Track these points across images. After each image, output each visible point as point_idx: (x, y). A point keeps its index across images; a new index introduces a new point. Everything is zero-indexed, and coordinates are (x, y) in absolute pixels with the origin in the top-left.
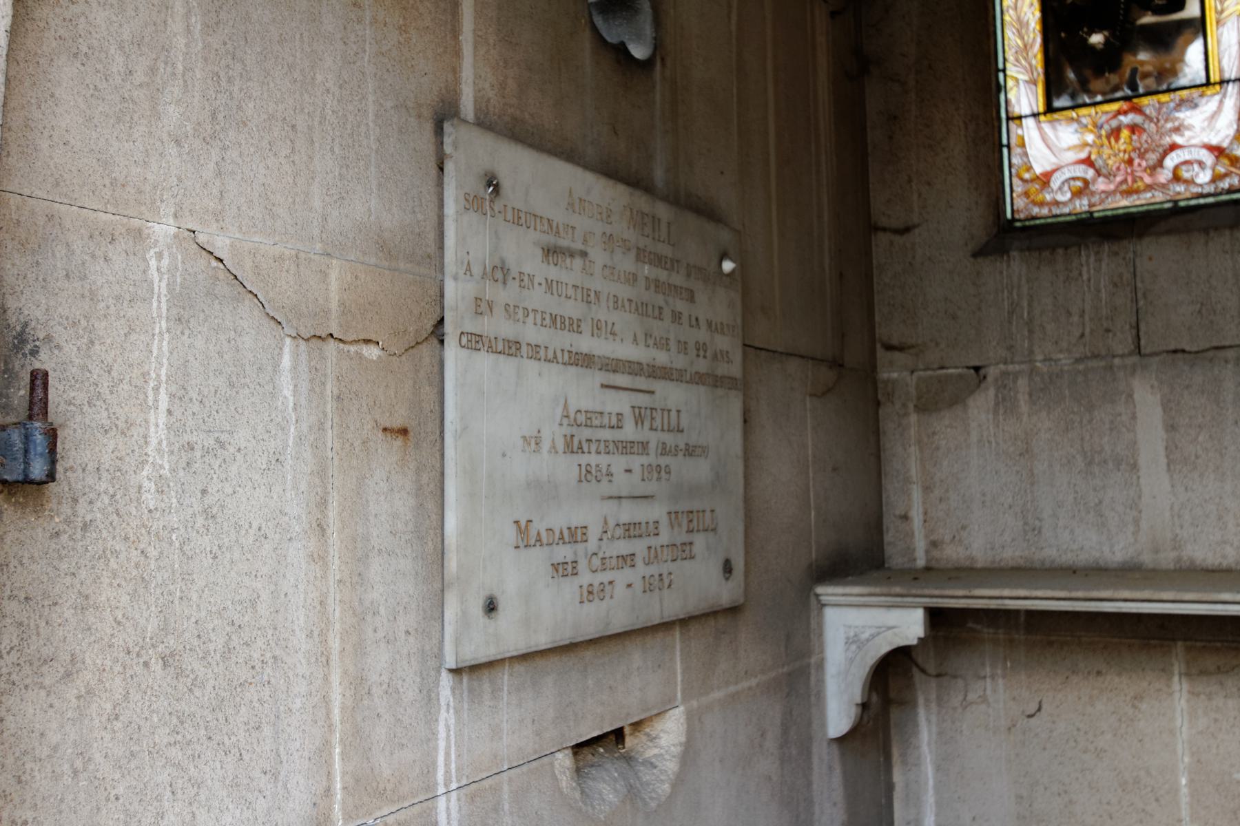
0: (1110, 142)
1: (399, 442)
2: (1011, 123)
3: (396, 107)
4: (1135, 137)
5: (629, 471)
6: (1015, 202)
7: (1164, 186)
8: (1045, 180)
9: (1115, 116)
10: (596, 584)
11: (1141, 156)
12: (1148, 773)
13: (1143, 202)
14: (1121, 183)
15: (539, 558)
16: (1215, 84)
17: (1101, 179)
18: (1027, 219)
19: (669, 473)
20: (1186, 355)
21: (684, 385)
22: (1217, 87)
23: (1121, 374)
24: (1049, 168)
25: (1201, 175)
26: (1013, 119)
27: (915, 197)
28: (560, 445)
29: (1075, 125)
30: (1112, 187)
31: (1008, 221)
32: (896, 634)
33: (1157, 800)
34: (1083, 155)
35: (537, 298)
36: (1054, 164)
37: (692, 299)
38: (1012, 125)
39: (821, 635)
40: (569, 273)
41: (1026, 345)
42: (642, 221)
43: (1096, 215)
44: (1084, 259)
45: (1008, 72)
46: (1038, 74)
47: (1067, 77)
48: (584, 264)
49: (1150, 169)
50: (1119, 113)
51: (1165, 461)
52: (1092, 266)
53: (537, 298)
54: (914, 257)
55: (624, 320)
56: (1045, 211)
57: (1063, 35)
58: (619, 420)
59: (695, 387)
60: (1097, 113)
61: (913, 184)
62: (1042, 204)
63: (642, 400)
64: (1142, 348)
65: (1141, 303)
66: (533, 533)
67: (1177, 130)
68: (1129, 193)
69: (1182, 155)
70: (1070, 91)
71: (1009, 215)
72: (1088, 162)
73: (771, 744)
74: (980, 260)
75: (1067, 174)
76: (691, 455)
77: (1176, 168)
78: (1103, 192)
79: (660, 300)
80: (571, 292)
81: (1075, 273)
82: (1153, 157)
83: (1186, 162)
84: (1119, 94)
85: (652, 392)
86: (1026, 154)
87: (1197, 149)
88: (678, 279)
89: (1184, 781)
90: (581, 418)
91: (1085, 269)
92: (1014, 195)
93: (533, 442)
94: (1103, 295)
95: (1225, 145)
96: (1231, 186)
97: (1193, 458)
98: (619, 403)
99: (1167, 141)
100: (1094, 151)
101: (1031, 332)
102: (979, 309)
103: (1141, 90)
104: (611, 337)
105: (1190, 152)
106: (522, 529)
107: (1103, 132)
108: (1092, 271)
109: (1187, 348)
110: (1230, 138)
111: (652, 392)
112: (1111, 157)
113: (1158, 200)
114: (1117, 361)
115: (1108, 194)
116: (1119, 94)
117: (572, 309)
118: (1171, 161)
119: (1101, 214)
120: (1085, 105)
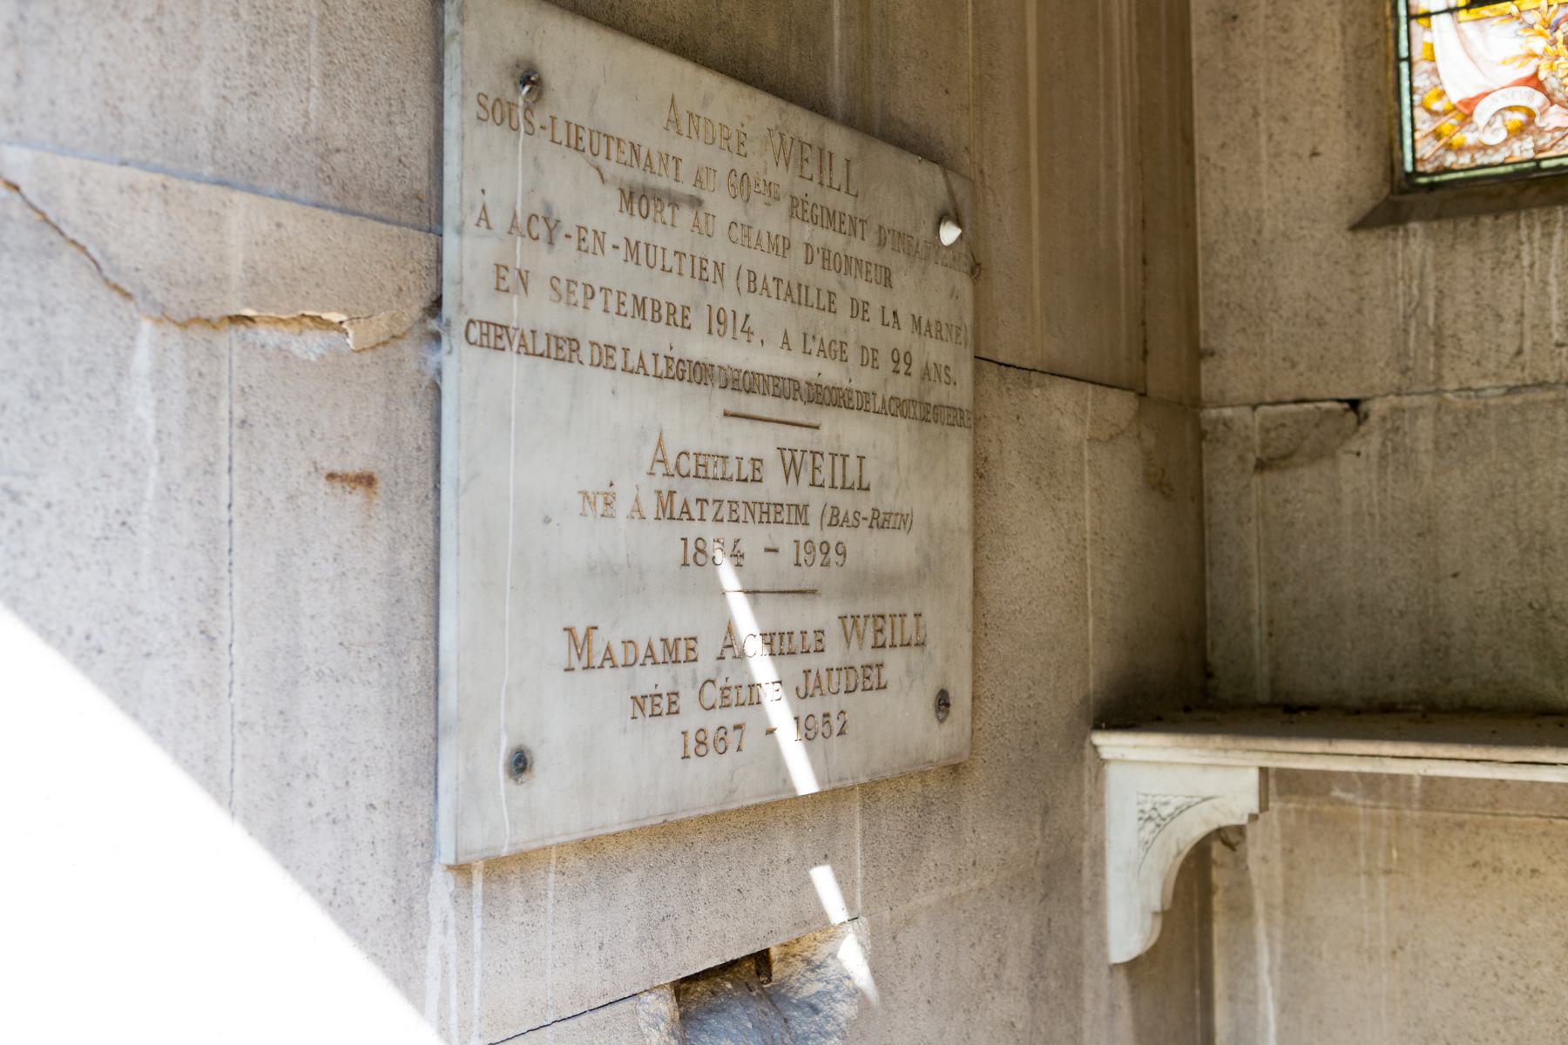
6: (1418, 145)
8: (1465, 110)
15: (610, 688)
18: (1437, 172)
21: (873, 416)
27: (1263, 139)
28: (650, 506)
29: (1515, 25)
32: (1215, 808)
34: (1527, 72)
37: (888, 282)
41: (1431, 367)
42: (798, 154)
43: (1545, 164)
44: (1524, 232)
52: (1536, 245)
53: (609, 269)
54: (1260, 232)
55: (766, 311)
56: (1465, 160)
61: (1260, 120)
62: (1460, 150)
63: (795, 438)
72: (1534, 82)
74: (1362, 235)
78: (1558, 129)
81: (1509, 256)
86: (1435, 71)
91: (1526, 248)
92: (1418, 135)
100: (1544, 64)
101: (1439, 345)
102: (1359, 311)
108: (1537, 252)
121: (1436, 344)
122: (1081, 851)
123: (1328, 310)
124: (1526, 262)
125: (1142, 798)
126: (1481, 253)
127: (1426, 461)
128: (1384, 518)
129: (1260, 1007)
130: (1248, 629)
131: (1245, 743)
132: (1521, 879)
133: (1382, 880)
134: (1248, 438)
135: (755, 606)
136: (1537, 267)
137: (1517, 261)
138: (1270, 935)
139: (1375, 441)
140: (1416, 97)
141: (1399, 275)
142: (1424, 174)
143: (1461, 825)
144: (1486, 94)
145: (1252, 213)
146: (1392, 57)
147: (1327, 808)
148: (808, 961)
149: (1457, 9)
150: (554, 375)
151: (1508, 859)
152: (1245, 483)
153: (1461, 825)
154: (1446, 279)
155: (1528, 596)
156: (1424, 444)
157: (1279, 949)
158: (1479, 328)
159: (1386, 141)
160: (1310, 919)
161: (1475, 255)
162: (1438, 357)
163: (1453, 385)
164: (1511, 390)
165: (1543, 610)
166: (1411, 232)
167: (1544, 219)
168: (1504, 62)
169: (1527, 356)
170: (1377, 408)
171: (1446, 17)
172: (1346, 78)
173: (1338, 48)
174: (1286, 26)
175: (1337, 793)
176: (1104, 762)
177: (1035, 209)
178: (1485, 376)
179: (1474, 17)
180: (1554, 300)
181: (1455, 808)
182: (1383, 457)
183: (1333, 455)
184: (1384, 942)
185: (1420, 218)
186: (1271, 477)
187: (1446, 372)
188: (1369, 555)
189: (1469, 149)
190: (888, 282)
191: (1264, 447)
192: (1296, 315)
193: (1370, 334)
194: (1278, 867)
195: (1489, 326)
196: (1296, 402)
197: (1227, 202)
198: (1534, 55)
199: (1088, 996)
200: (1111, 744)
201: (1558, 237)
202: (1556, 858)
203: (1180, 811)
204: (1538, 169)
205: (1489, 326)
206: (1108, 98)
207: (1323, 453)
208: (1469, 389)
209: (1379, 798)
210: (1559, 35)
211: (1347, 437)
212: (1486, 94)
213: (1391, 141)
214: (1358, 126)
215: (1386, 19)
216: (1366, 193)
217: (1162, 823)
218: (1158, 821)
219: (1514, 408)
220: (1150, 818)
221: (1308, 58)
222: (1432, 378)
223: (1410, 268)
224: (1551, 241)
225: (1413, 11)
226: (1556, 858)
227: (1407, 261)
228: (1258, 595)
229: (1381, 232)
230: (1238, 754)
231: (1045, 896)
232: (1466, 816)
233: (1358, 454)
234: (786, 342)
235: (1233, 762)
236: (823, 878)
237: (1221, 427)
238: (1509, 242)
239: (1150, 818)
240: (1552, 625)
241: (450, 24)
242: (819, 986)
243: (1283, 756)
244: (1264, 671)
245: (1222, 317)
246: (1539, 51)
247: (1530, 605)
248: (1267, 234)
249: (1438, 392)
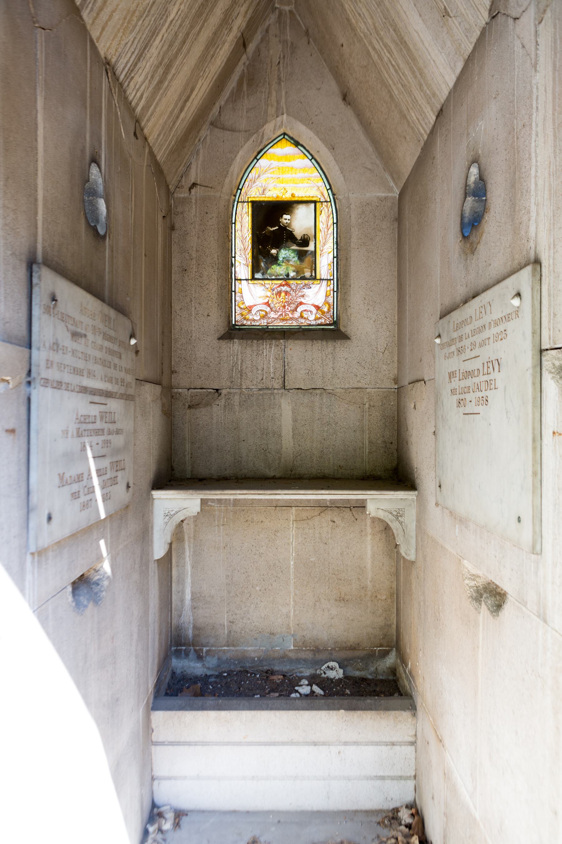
1: (11, 437)
2: (236, 281)
3: (11, 255)
4: (287, 297)
5: (97, 444)
7: (296, 319)
8: (250, 309)
9: (279, 287)
10: (86, 501)
11: (289, 305)
12: (279, 561)
13: (288, 324)
15: (67, 490)
16: (318, 280)
17: (272, 312)
19: (110, 443)
20: (302, 390)
21: (117, 400)
22: (319, 281)
23: (277, 397)
24: (251, 305)
25: (311, 316)
26: (238, 280)
27: (193, 309)
28: (75, 434)
29: (263, 287)
30: (276, 316)
32: (187, 511)
33: (282, 572)
34: (266, 301)
35: (69, 360)
37: (120, 358)
38: (237, 282)
39: (152, 513)
40: (79, 346)
41: (239, 381)
42: (106, 319)
44: (265, 346)
46: (249, 262)
47: (261, 266)
48: (85, 341)
50: (281, 285)
51: (292, 434)
52: (267, 350)
53: (69, 360)
54: (191, 336)
55: (98, 369)
56: (249, 323)
58: (95, 419)
59: (120, 400)
60: (272, 284)
61: (193, 303)
62: (248, 320)
63: (102, 408)
64: (286, 386)
65: (286, 367)
66: (65, 479)
67: (303, 296)
68: (283, 320)
70: (262, 271)
71: (234, 323)
72: (267, 304)
73: (137, 566)
74: (221, 341)
75: (259, 308)
76: (118, 434)
77: (302, 312)
78: (273, 318)
79: (109, 358)
80: (80, 355)
81: (261, 352)
82: (293, 306)
83: (305, 310)
85: (106, 404)
86: (242, 296)
88: (116, 348)
89: (292, 563)
90: (82, 419)
91: (265, 350)
92: (236, 314)
93: (65, 432)
94: (271, 363)
95: (320, 306)
97: (302, 433)
98: (95, 411)
99: (299, 300)
100: (270, 300)
101: (241, 375)
102: (220, 363)
104: (93, 377)
106: (61, 477)
107: (274, 292)
108: (268, 352)
109: (302, 388)
110: (322, 303)
111: (106, 404)
112: (276, 303)
113: (294, 324)
114: (276, 391)
115: (276, 319)
117: (80, 364)
118: (300, 309)
120: (267, 279)
121: (240, 375)
122: (149, 527)
123: (211, 362)
125: (165, 509)
127: (237, 408)
128: (225, 424)
129: (186, 568)
130: (185, 456)
131: (198, 492)
132: (258, 524)
133: (222, 527)
134: (186, 398)
135: (95, 461)
138: (189, 546)
139: (223, 401)
140: (236, 303)
142: (237, 325)
143: (243, 510)
144: (255, 305)
145: (189, 331)
146: (230, 290)
147: (207, 508)
148: (95, 570)
149: (248, 280)
150: (57, 393)
151: (255, 519)
152: (185, 412)
153: (243, 510)
155: (262, 447)
156: (236, 403)
157: (192, 550)
158: (252, 372)
160: (201, 540)
161: (252, 351)
162: (241, 379)
163: (245, 387)
164: (260, 390)
165: (266, 450)
169: (264, 380)
170: (224, 392)
173: (216, 285)
174: (201, 276)
175: (209, 503)
176: (154, 499)
177: (143, 329)
178: (253, 385)
180: (271, 366)
181: (242, 505)
182: (225, 406)
183: (211, 405)
184: (222, 545)
185: (237, 338)
186: (192, 410)
187: (243, 383)
188: (220, 434)
189: (250, 320)
190: (120, 358)
191: (191, 402)
192: (201, 363)
193: (222, 370)
194: (192, 526)
195: (255, 371)
196: (201, 389)
197: (182, 326)
198: (268, 297)
199: (150, 570)
200: (157, 494)
202: (267, 517)
203: (177, 513)
205: (255, 371)
206: (157, 294)
207: (208, 404)
208: (249, 388)
209: (222, 504)
210: (274, 292)
211: (215, 400)
212: (255, 305)
214: (221, 309)
216: (222, 330)
217: (171, 517)
218: (170, 516)
219: (260, 394)
220: (167, 515)
221: (207, 287)
222: (239, 385)
225: (236, 278)
226: (267, 517)
228: (188, 446)
229: (227, 341)
230: (196, 495)
231: (143, 542)
232: (245, 508)
233: (218, 405)
234: (101, 379)
235: (194, 497)
236: (102, 543)
237: (178, 395)
238: (261, 348)
239: (167, 515)
240: (268, 454)
241: (35, 281)
242: (98, 577)
243: (209, 495)
244: (189, 468)
245: (179, 361)
246: (269, 296)
247: (263, 449)
248: (193, 337)
249: (241, 389)
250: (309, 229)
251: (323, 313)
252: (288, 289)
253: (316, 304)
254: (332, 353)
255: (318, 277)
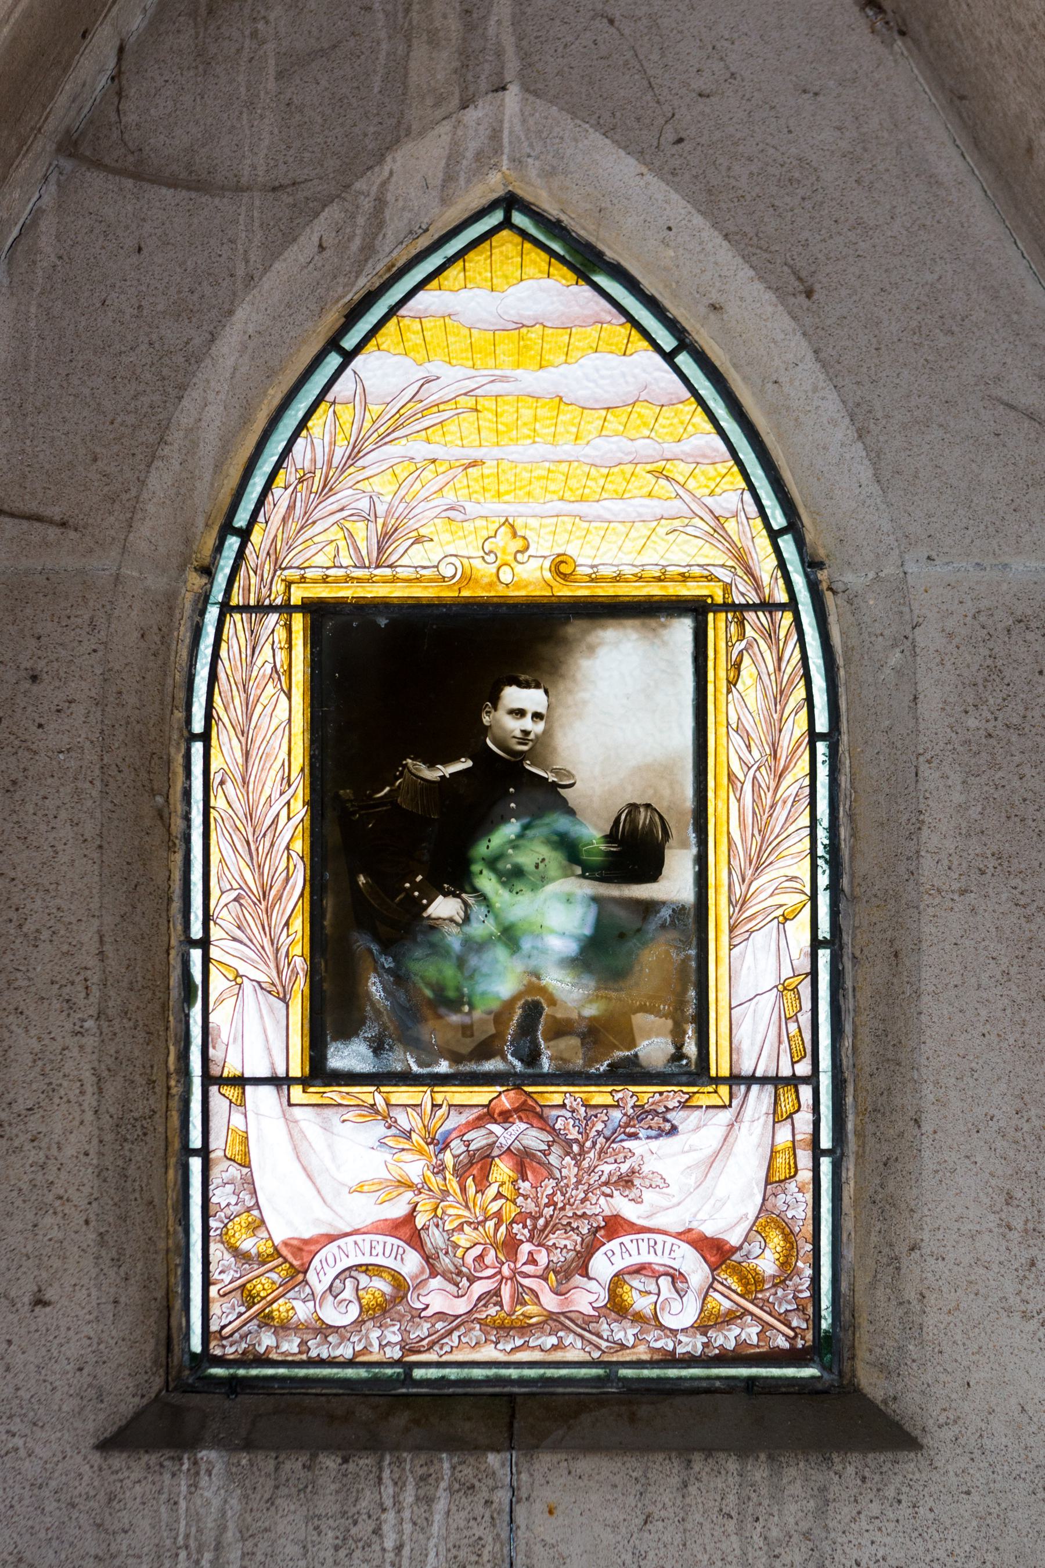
0: (463, 1189)
2: (214, 1089)
4: (525, 1186)
6: (215, 1309)
7: (585, 1324)
9: (478, 1123)
11: (538, 1236)
13: (536, 1356)
14: (487, 1298)
16: (718, 1080)
17: (436, 1282)
18: (242, 1362)
29: (379, 1129)
30: (461, 1307)
31: (194, 1355)
34: (398, 1210)
36: (317, 1221)
43: (418, 1373)
44: (388, 1490)
45: (214, 953)
47: (368, 995)
49: (556, 1273)
50: (489, 1115)
52: (406, 1514)
56: (291, 1346)
57: (362, 880)
60: (435, 1106)
62: (283, 1328)
67: (626, 1182)
68: (503, 1328)
69: (632, 1248)
70: (370, 1031)
71: (196, 1345)
74: (118, 1460)
77: (618, 1279)
78: (441, 1315)
82: (566, 1242)
83: (640, 1270)
84: (490, 1066)
86: (249, 1184)
87: (670, 1240)
91: (390, 1517)
92: (213, 1291)
95: (734, 1239)
96: (740, 1344)
99: (603, 1206)
100: (425, 1205)
103: (546, 1065)
105: (653, 1247)
107: (448, 1158)
108: (408, 1527)
110: (746, 1225)
115: (457, 1323)
116: (490, 1066)
119: (433, 1373)
120: (406, 1078)
124: (389, 1544)
126: (319, 1517)
136: (406, 1552)
137: (374, 1538)
141: (181, 1541)
142: (221, 1361)
144: (331, 1238)
146: (177, 1145)
154: (259, 1557)
159: (160, 1294)
161: (308, 1520)
166: (203, 1467)
167: (420, 1472)
168: (359, 1189)
171: (267, 1092)
172: (100, 1173)
173: (89, 1116)
179: (316, 1099)
185: (220, 1444)
198: (410, 1186)
201: (441, 1505)
204: (407, 1379)
210: (448, 1158)
212: (331, 1238)
213: (168, 1292)
214: (117, 1262)
215: (168, 1076)
221: (34, 1124)
223: (199, 1531)
224: (430, 1511)
227: (194, 1517)
229: (153, 1458)
250: (666, 770)
251: (752, 1283)
252: (534, 1139)
253: (709, 1230)
254: (807, 1535)
255: (720, 1065)
